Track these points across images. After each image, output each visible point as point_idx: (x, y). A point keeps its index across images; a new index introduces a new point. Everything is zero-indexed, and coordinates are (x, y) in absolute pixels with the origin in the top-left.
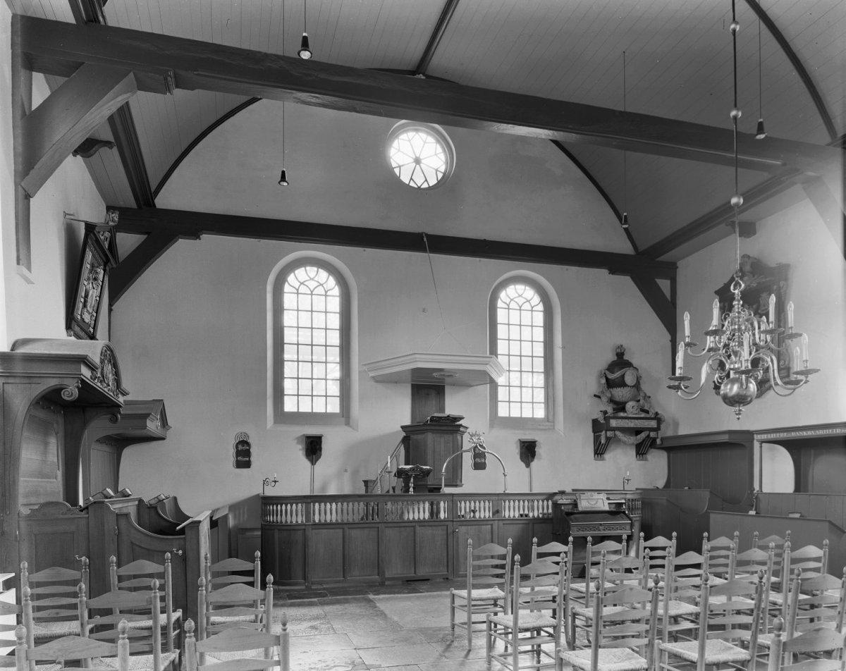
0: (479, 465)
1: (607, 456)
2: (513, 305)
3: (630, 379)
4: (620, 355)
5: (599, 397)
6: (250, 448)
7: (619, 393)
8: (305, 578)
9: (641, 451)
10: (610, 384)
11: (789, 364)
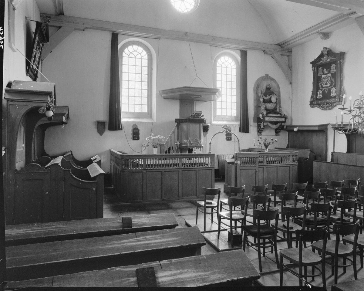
2: (223, 65)
3: (274, 99)
9: (277, 131)
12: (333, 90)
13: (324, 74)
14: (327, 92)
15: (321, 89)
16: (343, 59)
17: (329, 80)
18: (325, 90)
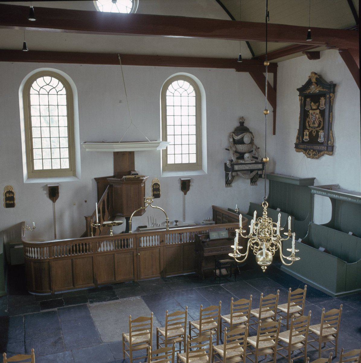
0: (156, 195)
1: (233, 184)
3: (247, 139)
4: (242, 123)
5: (229, 150)
6: (14, 195)
7: (240, 148)
8: (50, 288)
9: (253, 181)
10: (236, 142)
11: (333, 144)
12: (321, 134)
13: (312, 109)
14: (314, 134)
15: (307, 129)
16: (334, 92)
17: (317, 118)
18: (312, 131)
